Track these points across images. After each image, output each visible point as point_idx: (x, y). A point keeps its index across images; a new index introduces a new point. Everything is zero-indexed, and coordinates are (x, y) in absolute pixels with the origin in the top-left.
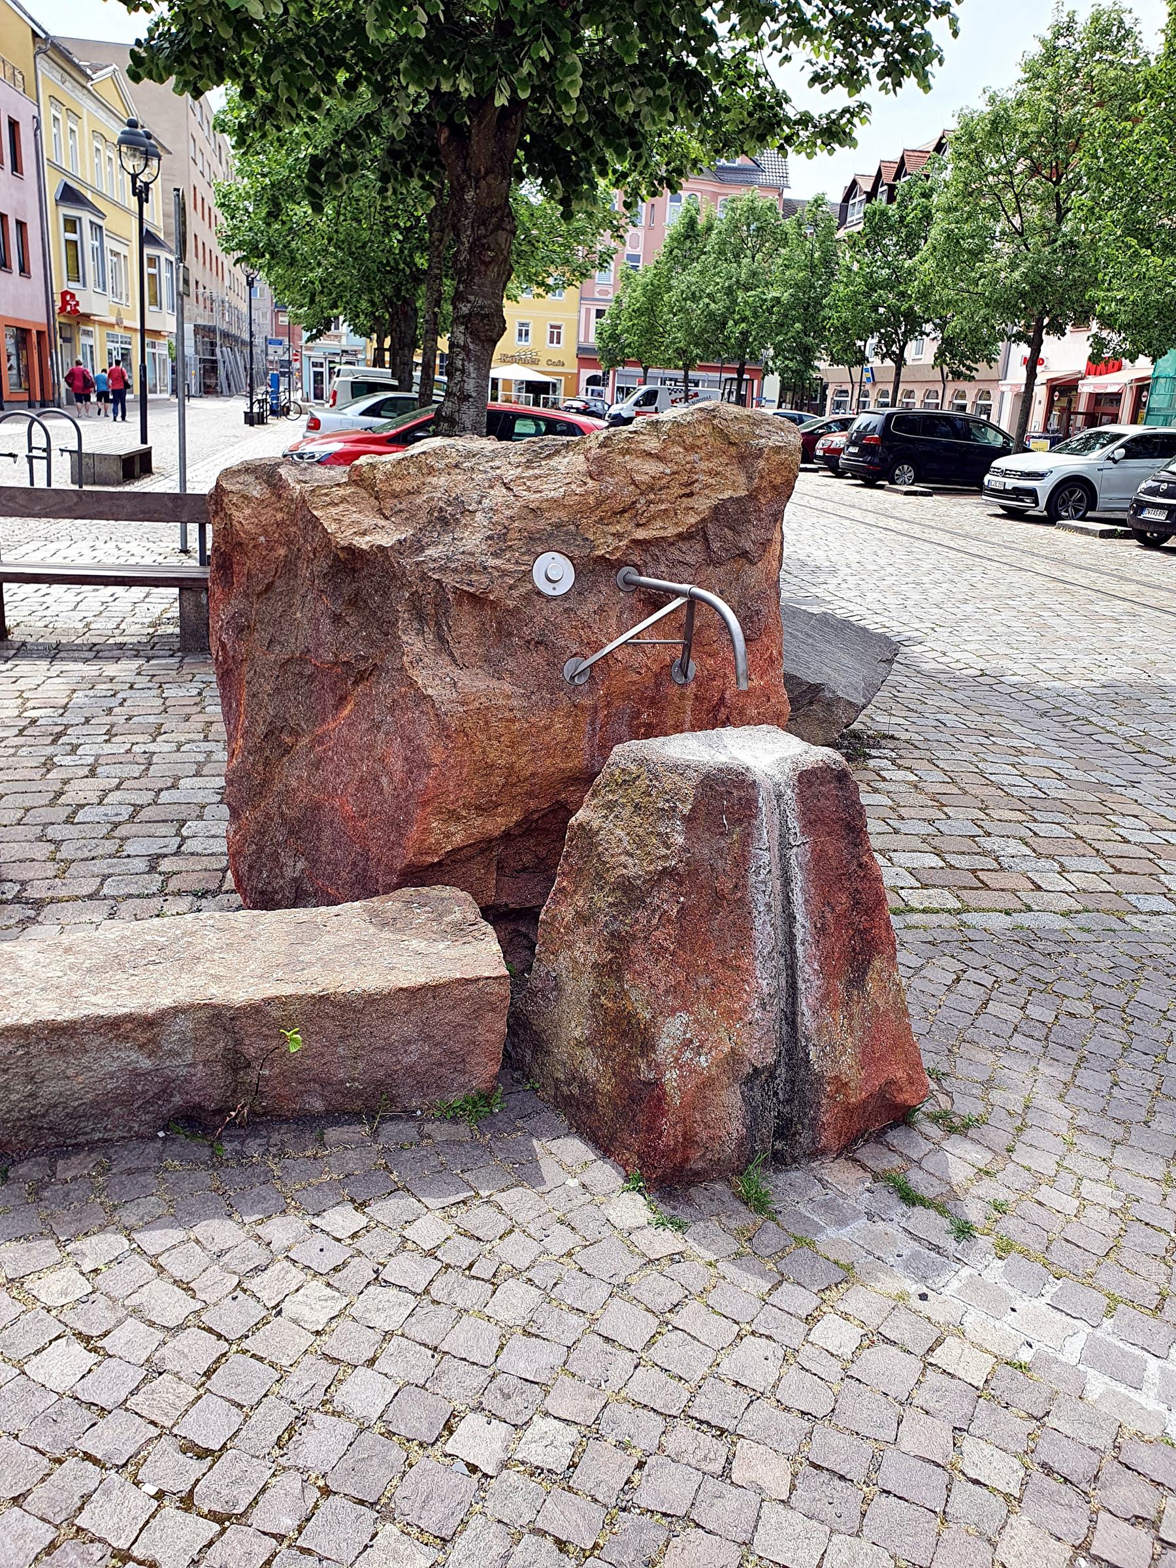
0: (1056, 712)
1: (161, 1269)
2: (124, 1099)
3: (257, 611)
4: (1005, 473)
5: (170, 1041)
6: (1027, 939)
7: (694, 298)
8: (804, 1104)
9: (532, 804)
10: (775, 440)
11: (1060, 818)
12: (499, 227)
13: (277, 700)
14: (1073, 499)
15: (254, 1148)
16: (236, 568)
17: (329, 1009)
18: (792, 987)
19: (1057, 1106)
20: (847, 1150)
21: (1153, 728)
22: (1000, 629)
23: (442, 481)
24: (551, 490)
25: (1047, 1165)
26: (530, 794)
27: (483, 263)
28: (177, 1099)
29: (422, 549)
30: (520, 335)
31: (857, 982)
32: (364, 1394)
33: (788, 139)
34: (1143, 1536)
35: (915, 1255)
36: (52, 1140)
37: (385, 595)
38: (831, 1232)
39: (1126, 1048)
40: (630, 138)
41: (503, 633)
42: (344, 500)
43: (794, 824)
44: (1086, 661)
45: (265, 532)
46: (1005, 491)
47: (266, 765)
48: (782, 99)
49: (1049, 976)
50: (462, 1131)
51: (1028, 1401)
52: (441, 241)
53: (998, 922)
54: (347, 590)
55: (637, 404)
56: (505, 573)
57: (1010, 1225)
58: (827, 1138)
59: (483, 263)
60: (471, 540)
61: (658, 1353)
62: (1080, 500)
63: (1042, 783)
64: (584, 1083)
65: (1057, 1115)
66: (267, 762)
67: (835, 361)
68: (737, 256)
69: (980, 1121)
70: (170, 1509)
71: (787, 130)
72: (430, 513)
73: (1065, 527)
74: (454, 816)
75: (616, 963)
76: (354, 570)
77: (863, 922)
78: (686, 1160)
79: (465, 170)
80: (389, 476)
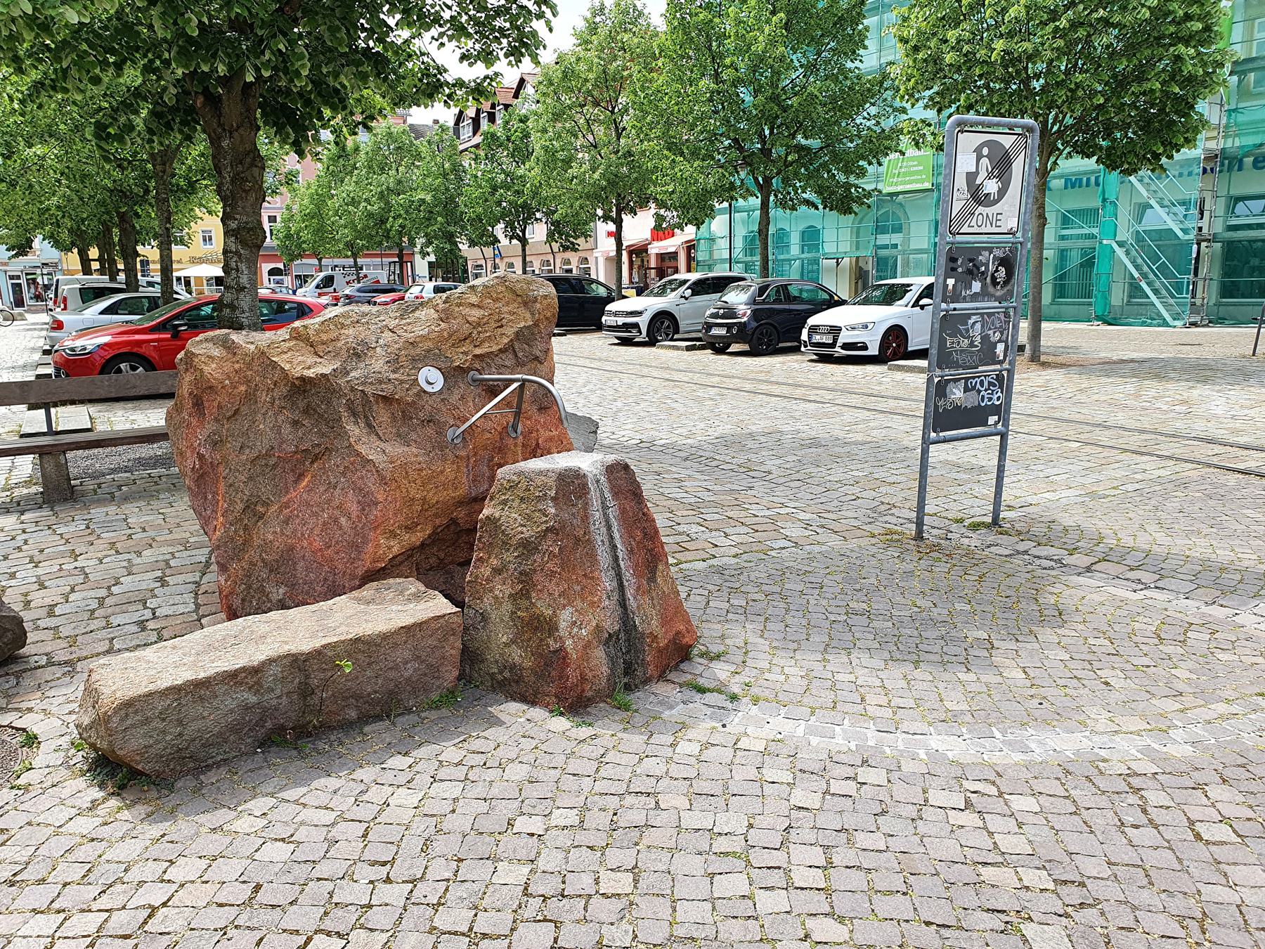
0: (692, 456)
1: (304, 805)
2: (235, 729)
3: (228, 430)
4: (616, 314)
5: (268, 681)
6: (720, 571)
7: (354, 202)
8: (637, 651)
9: (438, 522)
10: (542, 292)
11: (715, 510)
12: (253, 165)
13: (251, 485)
14: (663, 327)
15: (321, 745)
16: (206, 404)
17: (361, 646)
18: (621, 587)
19: (761, 641)
20: (662, 677)
21: (752, 456)
22: (642, 414)
23: (351, 331)
24: (420, 330)
25: (765, 665)
26: (436, 516)
27: (244, 191)
28: (269, 725)
29: (348, 373)
30: (205, 240)
31: (652, 579)
32: (460, 822)
33: (449, 96)
34: (852, 784)
35: (713, 713)
36: (191, 765)
37: (329, 403)
38: (667, 713)
39: (787, 610)
40: (338, 100)
41: (406, 417)
42: (290, 349)
43: (608, 495)
44: (702, 425)
45: (229, 378)
46: (618, 326)
47: (245, 530)
48: (442, 70)
49: (738, 585)
50: (444, 712)
51: (785, 751)
52: (164, 172)
53: (700, 565)
54: (302, 404)
55: (317, 287)
56: (402, 382)
57: (755, 690)
58: (651, 670)
59: (244, 191)
60: (377, 364)
61: (603, 773)
62: (668, 327)
63: (699, 495)
64: (513, 667)
65: (763, 644)
66: (246, 528)
67: (473, 243)
68: (382, 169)
69: (725, 653)
70: (380, 885)
71: (447, 91)
72: (348, 351)
73: (662, 347)
74: (393, 535)
75: (525, 585)
76: (305, 391)
77: (649, 545)
78: (583, 691)
79: (220, 125)
80: (318, 332)
